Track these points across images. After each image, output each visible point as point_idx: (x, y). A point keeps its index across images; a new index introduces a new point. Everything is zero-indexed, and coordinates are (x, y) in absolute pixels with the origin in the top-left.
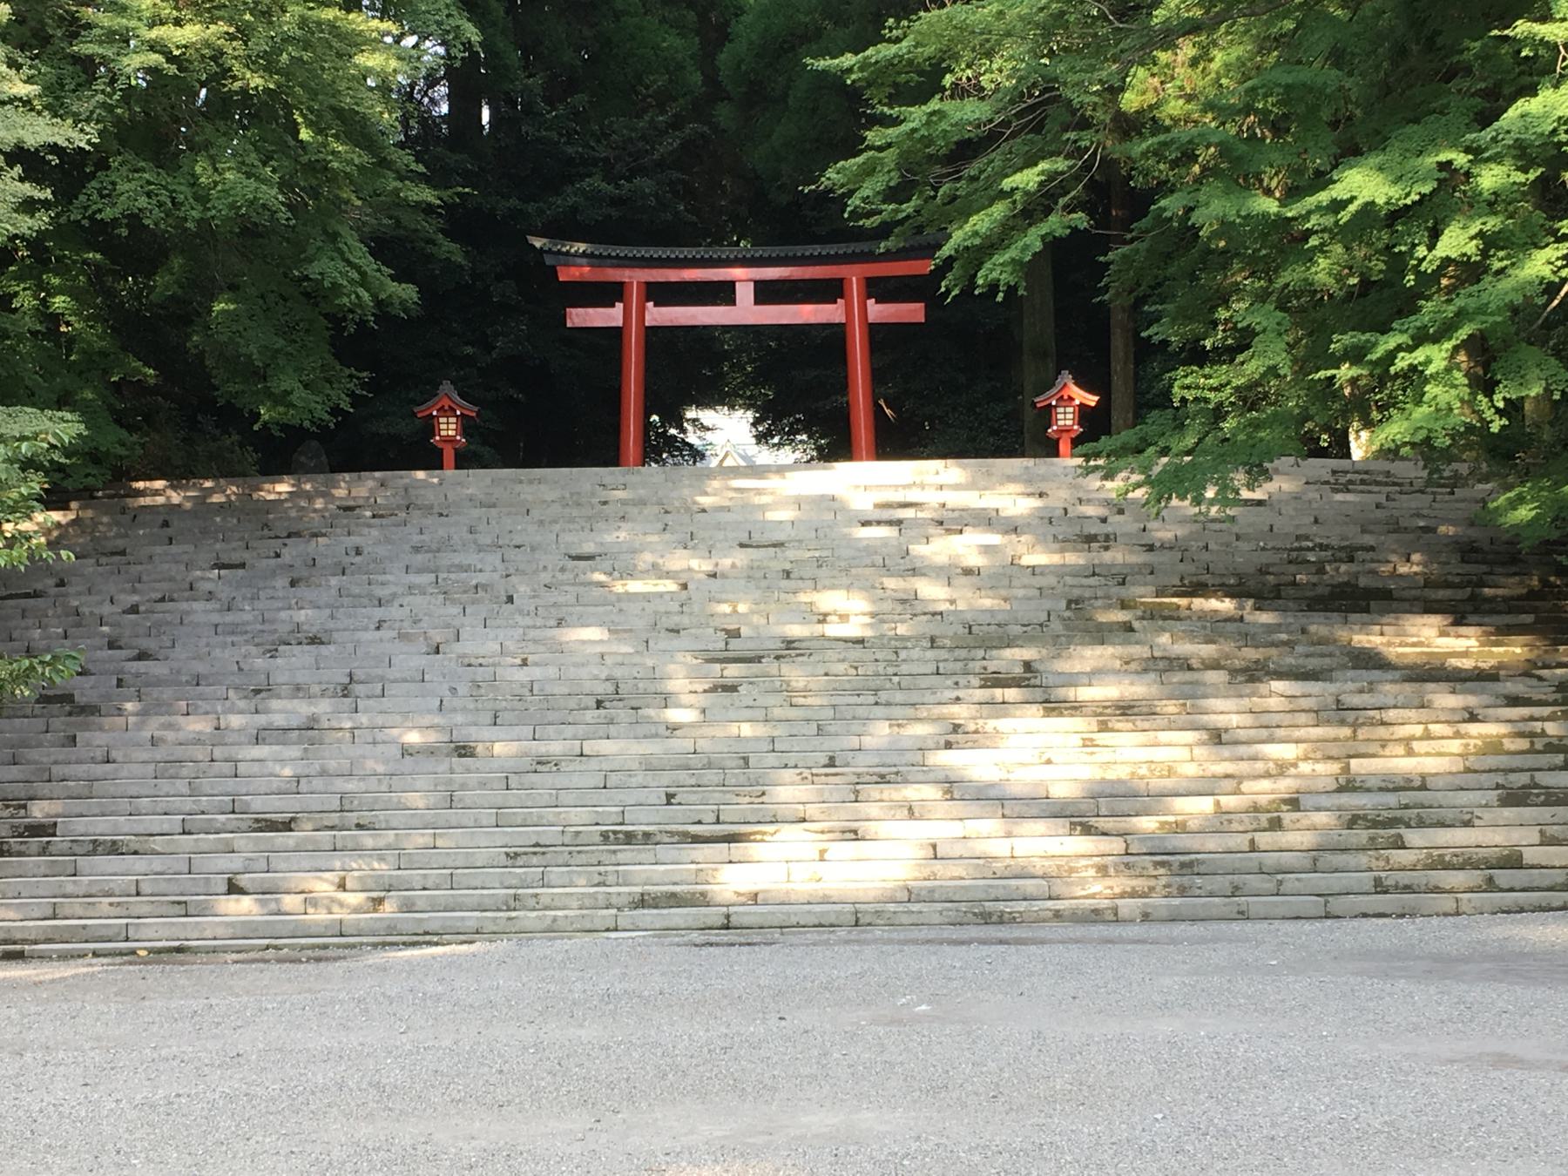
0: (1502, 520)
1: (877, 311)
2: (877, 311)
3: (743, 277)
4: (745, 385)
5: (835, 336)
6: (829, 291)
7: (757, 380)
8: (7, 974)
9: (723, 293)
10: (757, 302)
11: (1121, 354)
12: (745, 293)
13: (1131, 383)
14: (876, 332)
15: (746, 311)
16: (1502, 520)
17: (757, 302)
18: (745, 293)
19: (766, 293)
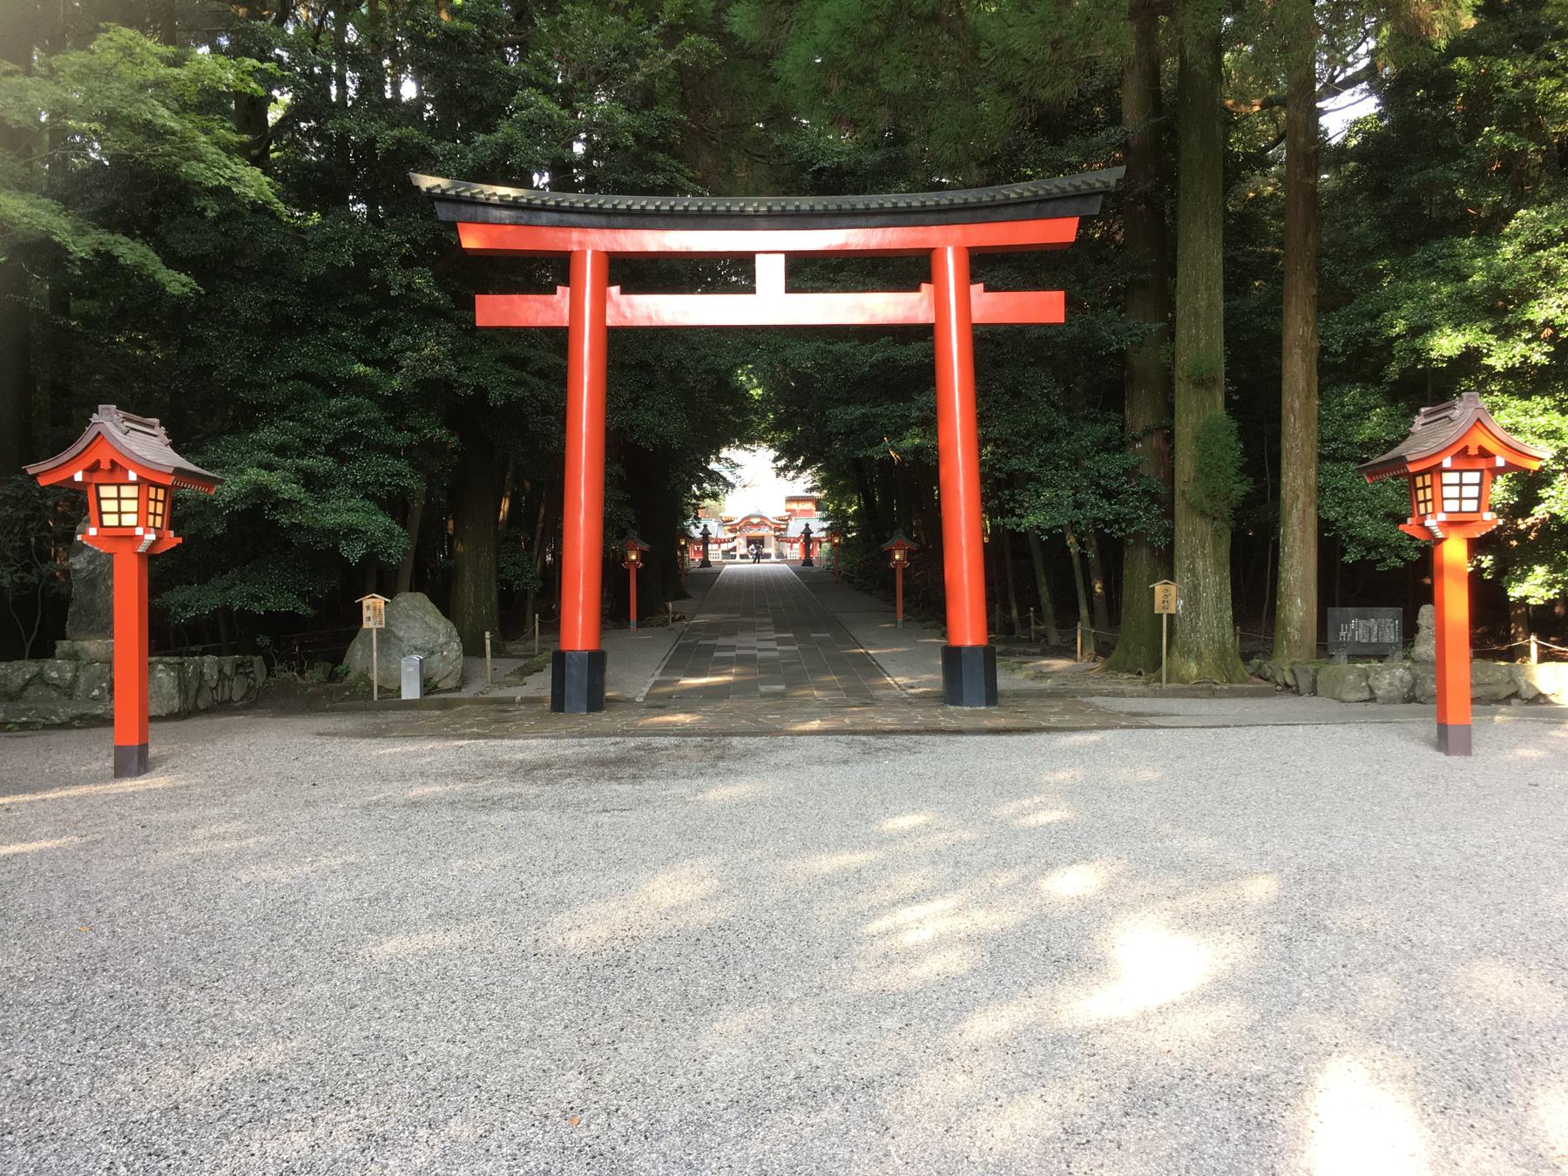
0: (1120, 866)
1: (990, 306)
2: (990, 306)
3: (772, 247)
4: (767, 430)
5: (921, 335)
6: (905, 270)
7: (778, 426)
8: (582, 544)
9: (733, 273)
10: (790, 289)
11: (1301, 384)
12: (770, 272)
13: (1314, 426)
14: (990, 344)
15: (769, 304)
16: (1120, 866)
17: (790, 289)
18: (770, 272)
19: (806, 272)
